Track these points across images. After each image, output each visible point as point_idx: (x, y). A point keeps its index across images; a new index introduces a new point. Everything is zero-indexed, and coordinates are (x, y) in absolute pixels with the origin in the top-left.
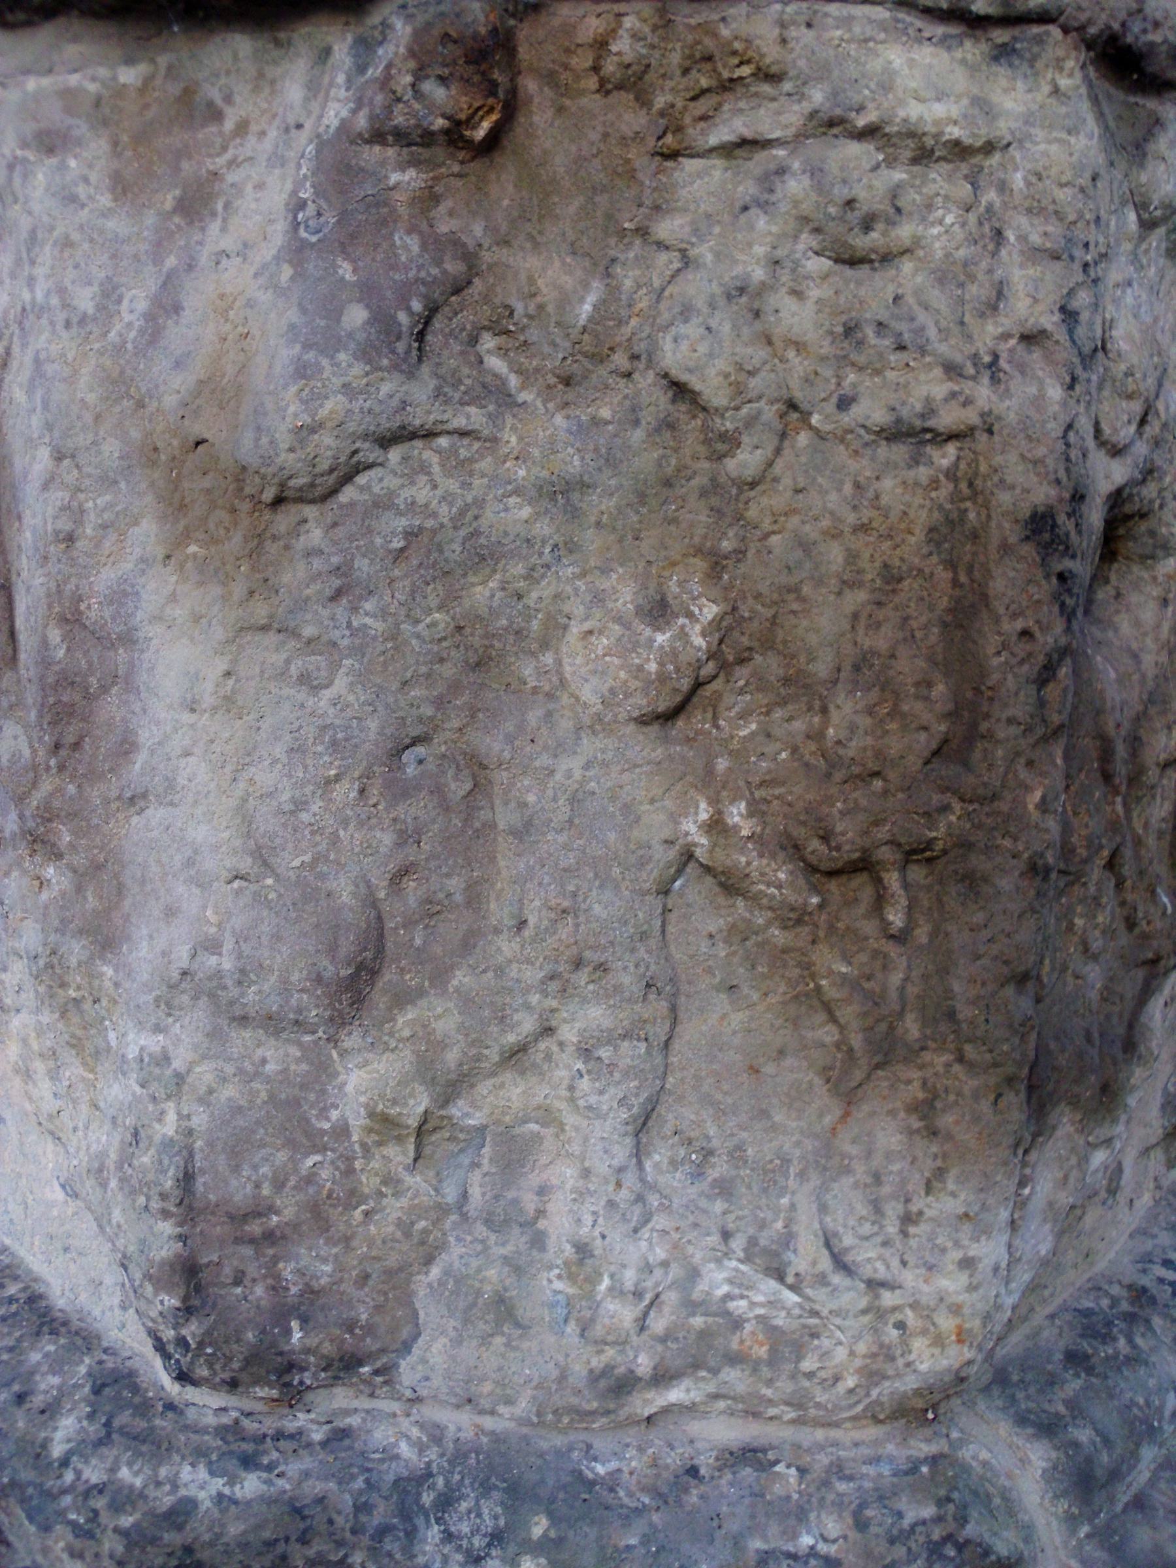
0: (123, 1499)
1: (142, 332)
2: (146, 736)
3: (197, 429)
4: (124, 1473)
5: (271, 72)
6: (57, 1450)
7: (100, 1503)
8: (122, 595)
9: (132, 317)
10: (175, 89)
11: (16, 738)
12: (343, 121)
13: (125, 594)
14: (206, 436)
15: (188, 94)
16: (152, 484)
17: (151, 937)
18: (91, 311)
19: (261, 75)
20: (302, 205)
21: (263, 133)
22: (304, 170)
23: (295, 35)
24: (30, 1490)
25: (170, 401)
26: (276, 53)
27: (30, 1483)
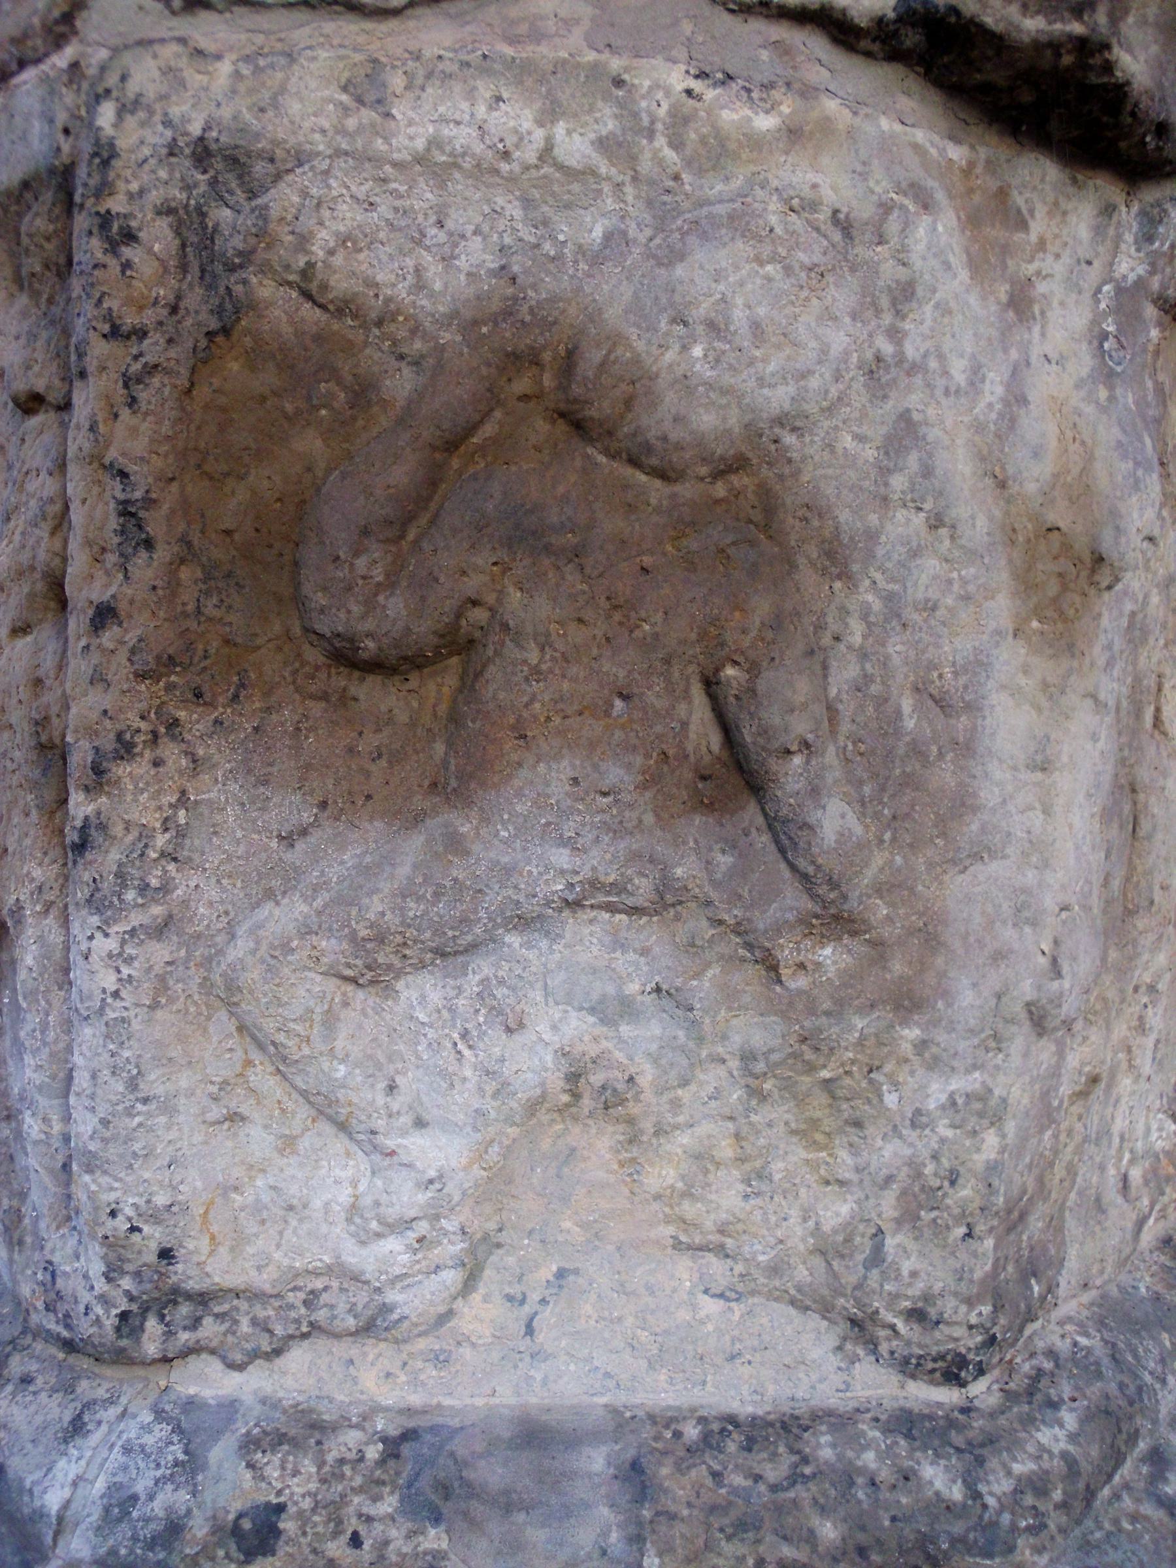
0: (1038, 1485)
1: (1001, 415)
2: (989, 795)
3: (1052, 518)
4: (1017, 1468)
5: (1064, 204)
6: (957, 1493)
7: (1029, 1500)
8: (978, 664)
9: (992, 399)
10: (993, 184)
11: (843, 816)
12: (1140, 278)
13: (980, 663)
14: (1061, 524)
15: (1002, 194)
16: (1010, 561)
17: (975, 985)
18: (963, 384)
19: (1056, 204)
20: (1104, 336)
21: (1058, 256)
22: (1103, 306)
23: (1091, 183)
24: (971, 1536)
25: (1031, 488)
26: (1071, 190)
27: (968, 1530)
